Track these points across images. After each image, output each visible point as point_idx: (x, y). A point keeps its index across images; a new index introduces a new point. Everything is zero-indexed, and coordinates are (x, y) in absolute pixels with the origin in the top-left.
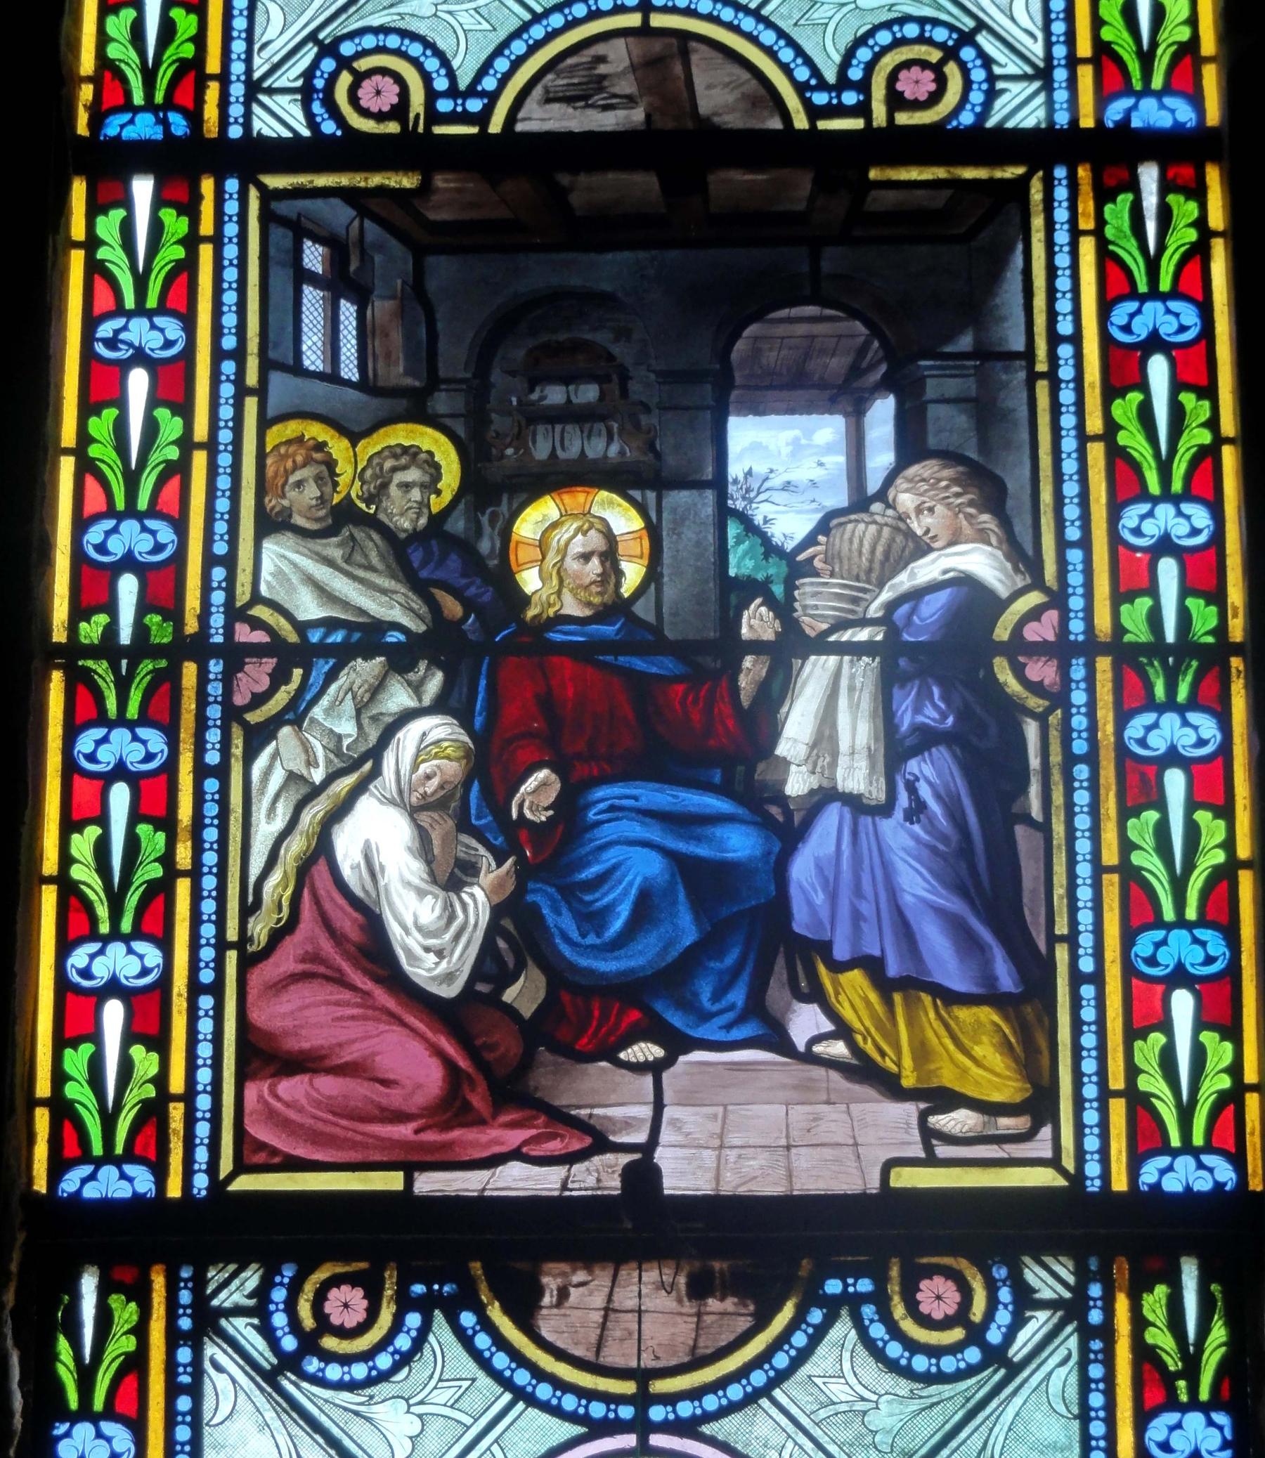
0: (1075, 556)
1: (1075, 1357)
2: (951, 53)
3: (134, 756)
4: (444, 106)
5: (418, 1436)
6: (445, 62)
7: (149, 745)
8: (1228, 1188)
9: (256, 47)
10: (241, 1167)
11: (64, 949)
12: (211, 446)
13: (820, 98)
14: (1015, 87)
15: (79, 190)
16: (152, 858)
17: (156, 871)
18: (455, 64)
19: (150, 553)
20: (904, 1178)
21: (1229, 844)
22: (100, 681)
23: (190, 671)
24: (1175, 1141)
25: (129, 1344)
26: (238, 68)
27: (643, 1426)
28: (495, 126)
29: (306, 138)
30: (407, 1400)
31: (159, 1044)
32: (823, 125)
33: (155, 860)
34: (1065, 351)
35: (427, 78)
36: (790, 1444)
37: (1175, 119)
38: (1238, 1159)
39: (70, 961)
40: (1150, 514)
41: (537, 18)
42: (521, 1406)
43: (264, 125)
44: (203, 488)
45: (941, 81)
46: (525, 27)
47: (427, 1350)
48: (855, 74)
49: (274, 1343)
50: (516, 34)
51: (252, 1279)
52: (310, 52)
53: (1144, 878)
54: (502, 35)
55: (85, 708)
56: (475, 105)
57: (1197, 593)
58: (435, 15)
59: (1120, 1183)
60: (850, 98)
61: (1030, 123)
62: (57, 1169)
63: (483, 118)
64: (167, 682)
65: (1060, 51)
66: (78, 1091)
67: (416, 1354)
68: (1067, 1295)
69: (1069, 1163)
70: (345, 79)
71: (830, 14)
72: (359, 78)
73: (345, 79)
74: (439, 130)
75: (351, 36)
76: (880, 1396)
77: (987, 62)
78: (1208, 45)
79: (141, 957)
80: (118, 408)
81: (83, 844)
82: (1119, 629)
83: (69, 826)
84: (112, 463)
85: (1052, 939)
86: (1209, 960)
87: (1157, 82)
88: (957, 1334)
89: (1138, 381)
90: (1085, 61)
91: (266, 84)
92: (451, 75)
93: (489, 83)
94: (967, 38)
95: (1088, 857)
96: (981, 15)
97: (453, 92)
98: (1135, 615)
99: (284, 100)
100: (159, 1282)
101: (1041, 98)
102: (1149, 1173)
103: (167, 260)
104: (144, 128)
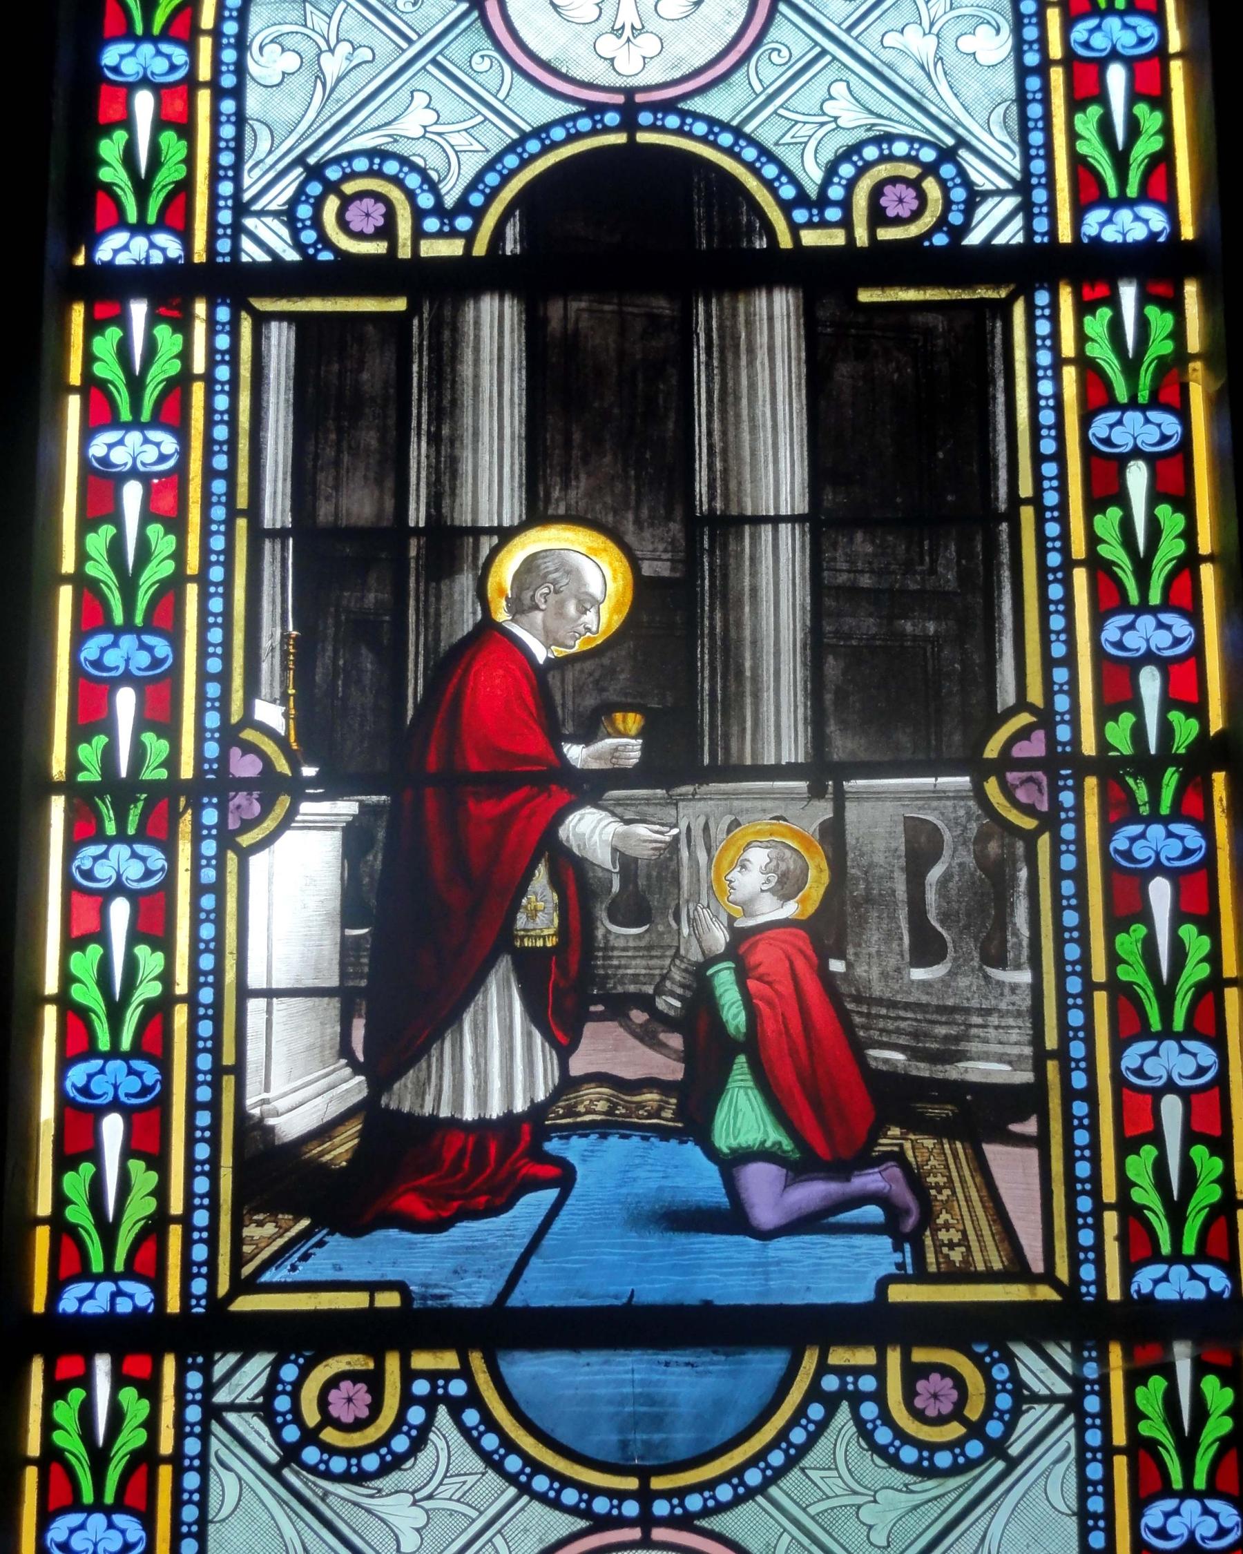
0: (1049, 469)
5: (424, 1527)
8: (1162, 239)
12: (202, 579)
15: (78, 313)
16: (156, 764)
20: (898, 1294)
27: (646, 1521)
29: (293, 263)
37: (1209, 1291)
38: (1230, 1268)
42: (525, 1499)
43: (251, 252)
48: (836, 193)
53: (1115, 574)
55: (69, 1265)
58: (423, 136)
59: (1065, 236)
62: (56, 1290)
66: (79, 1214)
69: (1062, 1273)
79: (123, 1532)
80: (108, 735)
81: (65, 1412)
82: (1103, 743)
83: (71, 944)
85: (1015, 501)
94: (947, 155)
96: (960, 130)
98: (1119, 734)
102: (1144, 1279)
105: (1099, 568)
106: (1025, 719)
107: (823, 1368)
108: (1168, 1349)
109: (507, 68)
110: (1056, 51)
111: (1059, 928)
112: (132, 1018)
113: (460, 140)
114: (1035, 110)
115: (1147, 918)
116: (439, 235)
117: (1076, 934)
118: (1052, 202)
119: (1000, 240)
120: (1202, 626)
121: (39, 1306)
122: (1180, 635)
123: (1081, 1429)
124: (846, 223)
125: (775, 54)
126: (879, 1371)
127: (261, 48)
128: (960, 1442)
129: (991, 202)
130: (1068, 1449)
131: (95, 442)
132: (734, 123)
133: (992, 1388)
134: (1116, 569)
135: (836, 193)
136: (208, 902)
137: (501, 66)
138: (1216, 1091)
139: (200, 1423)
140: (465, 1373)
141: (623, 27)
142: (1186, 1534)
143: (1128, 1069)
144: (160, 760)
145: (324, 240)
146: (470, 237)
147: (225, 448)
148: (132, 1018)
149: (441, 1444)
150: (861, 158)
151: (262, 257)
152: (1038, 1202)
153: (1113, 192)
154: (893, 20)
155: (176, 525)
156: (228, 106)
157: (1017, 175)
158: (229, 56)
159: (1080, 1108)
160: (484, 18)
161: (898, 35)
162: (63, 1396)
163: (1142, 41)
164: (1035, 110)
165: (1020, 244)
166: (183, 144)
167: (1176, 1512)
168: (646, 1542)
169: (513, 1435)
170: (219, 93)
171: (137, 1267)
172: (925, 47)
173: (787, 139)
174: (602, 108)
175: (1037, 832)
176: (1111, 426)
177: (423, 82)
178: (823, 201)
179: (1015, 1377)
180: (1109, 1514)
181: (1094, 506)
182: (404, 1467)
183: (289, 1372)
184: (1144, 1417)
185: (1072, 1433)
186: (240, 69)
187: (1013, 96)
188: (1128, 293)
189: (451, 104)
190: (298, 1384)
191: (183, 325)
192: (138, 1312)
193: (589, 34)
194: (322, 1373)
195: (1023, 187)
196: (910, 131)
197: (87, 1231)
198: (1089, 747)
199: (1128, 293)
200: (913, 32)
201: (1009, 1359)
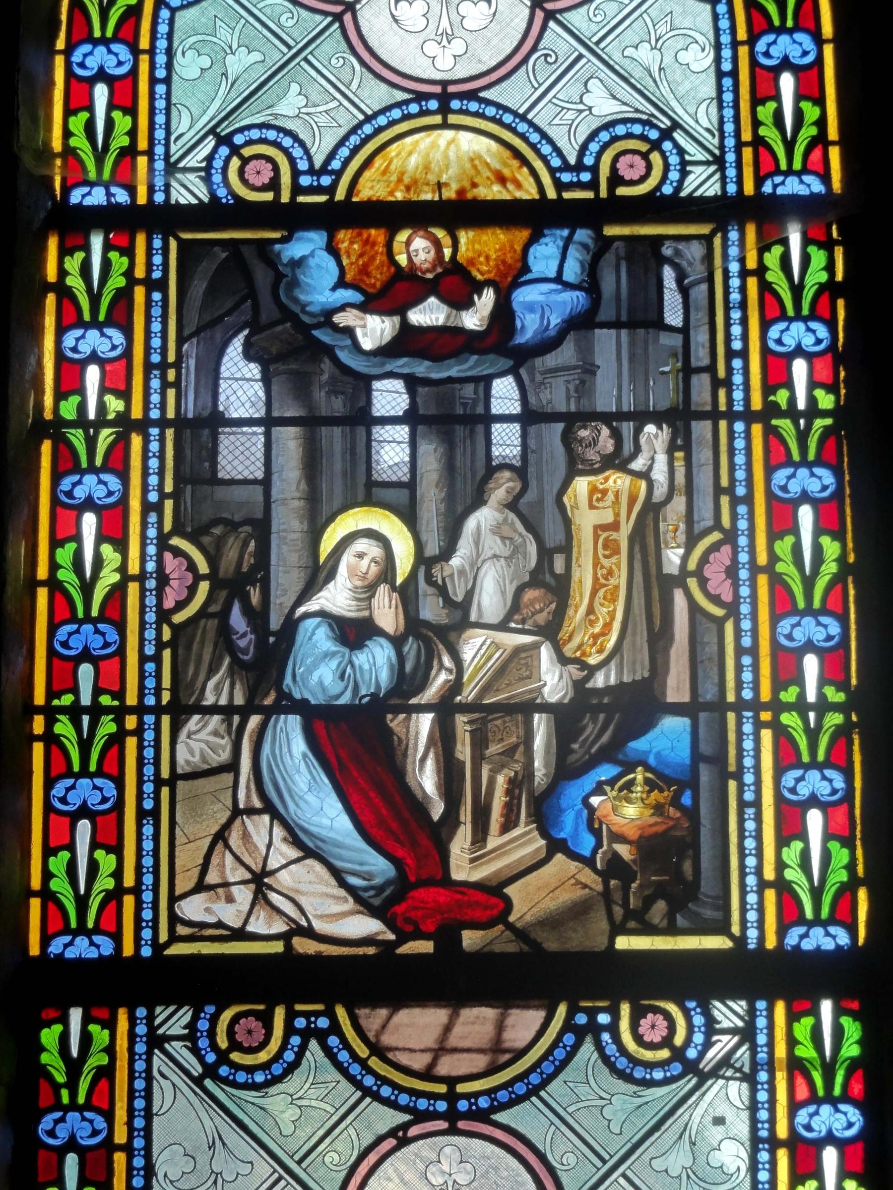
2: (656, 145)
3: (103, 348)
4: (305, 181)
6: (307, 152)
9: (173, 138)
10: (174, 938)
13: (566, 177)
14: (698, 170)
15: (53, 244)
17: (121, 282)
18: (313, 151)
23: (136, 441)
24: (806, 758)
26: (159, 150)
28: (340, 195)
30: (291, 1096)
31: (131, 111)
32: (567, 195)
33: (102, 1051)
34: (737, 363)
35: (292, 161)
36: (553, 1128)
39: (54, 792)
41: (368, 119)
42: (368, 1100)
43: (181, 197)
46: (360, 125)
47: (304, 1061)
49: (201, 1059)
50: (353, 131)
51: (185, 1015)
54: (342, 132)
55: (62, 613)
56: (326, 181)
57: (831, 683)
60: (586, 177)
61: (711, 193)
62: (46, 940)
63: (331, 190)
64: (121, 446)
65: (730, 142)
66: (59, 885)
68: (740, 1024)
71: (573, 117)
72: (245, 161)
74: (301, 199)
75: (241, 130)
76: (613, 1095)
77: (681, 152)
78: (833, 133)
83: (49, 852)
88: (665, 1054)
89: (773, 93)
91: (181, 165)
92: (310, 159)
93: (336, 165)
95: (734, 180)
97: (311, 171)
99: (192, 176)
101: (717, 176)
104: (97, 197)
106: (716, 536)
108: (784, 229)
113: (323, 120)
121: (34, 950)
127: (183, 53)
144: (125, 131)
149: (311, 1059)
160: (343, 28)
161: (634, 49)
165: (716, 196)
169: (361, 152)
173: (556, 121)
174: (427, 96)
181: (782, 841)
193: (416, 40)
194: (227, 1016)
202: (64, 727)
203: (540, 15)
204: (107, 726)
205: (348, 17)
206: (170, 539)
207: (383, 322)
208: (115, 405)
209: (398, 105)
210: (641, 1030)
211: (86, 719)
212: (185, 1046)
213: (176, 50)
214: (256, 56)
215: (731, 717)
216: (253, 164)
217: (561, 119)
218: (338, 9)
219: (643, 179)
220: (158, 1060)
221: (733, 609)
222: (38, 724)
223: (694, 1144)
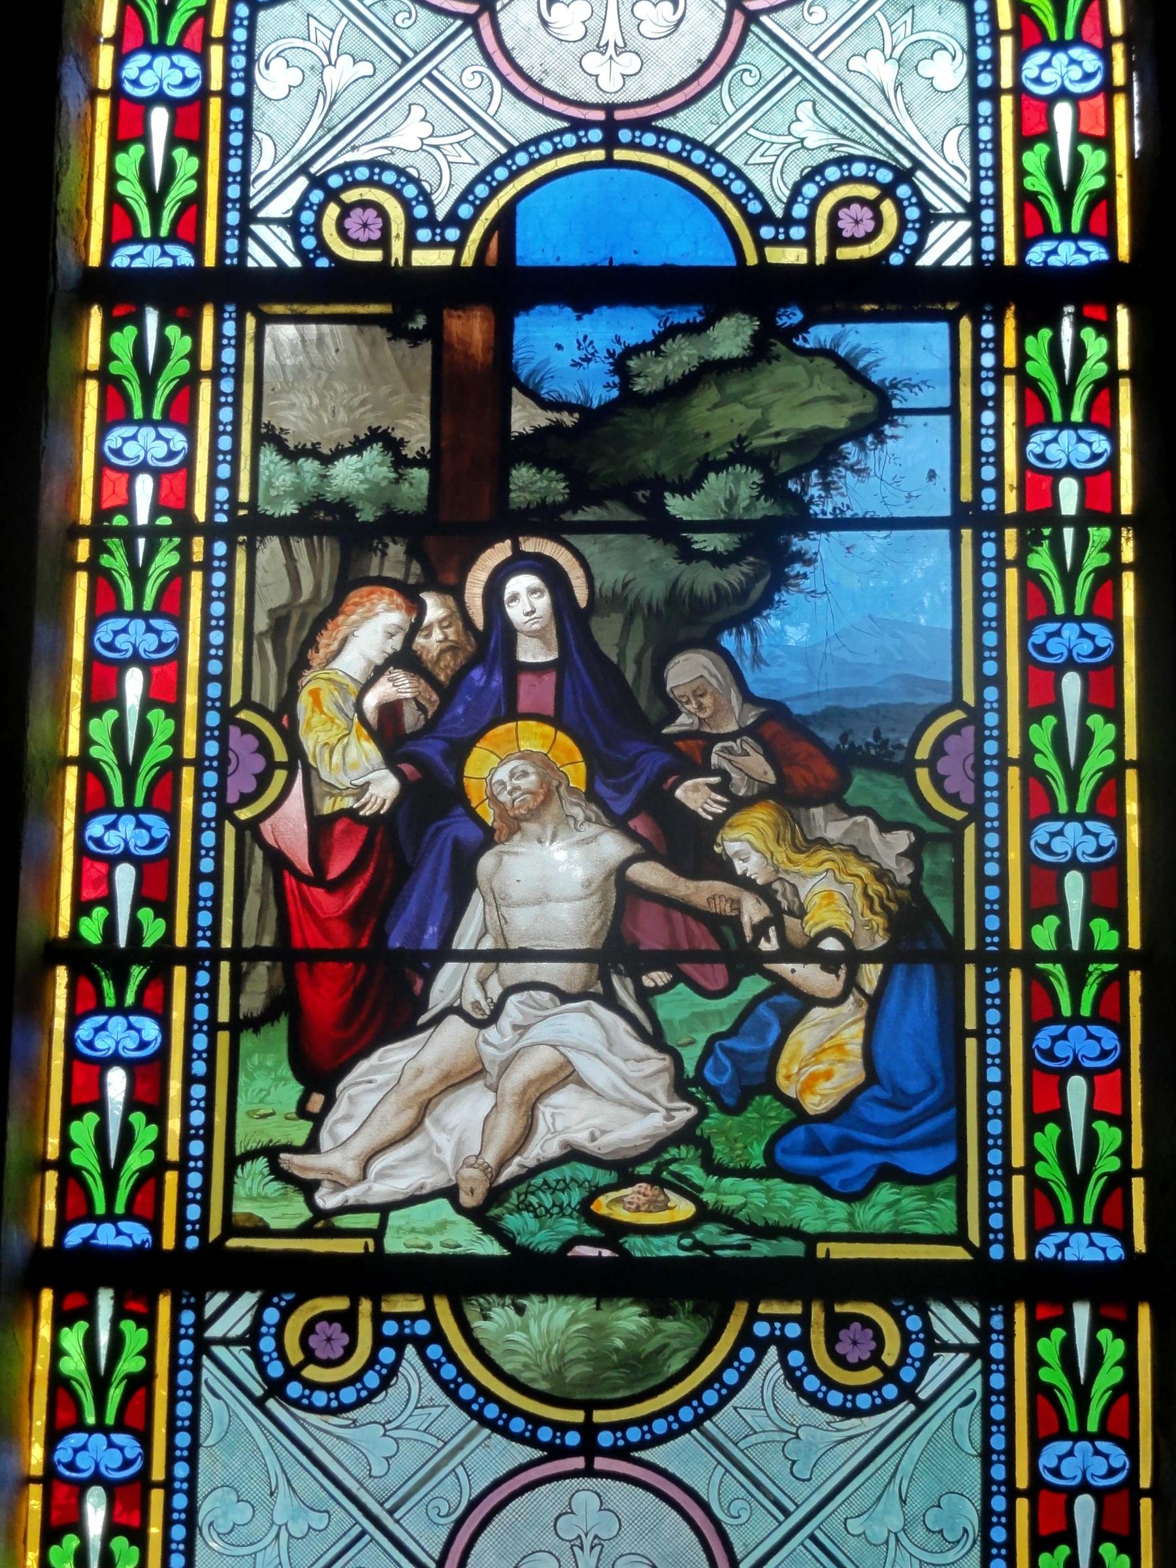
1: (979, 1396)
7: (144, 1034)
11: (74, 1021)
15: (96, 317)
19: (156, 651)
21: (1118, 745)
22: (107, 770)
25: (191, 187)
29: (296, 269)
40: (1064, 1036)
43: (257, 258)
44: (189, 840)
45: (878, 219)
48: (800, 211)
52: (302, 183)
53: (1039, 201)
67: (391, 1379)
69: (974, 1236)
70: (333, 211)
73: (333, 211)
79: (121, 1449)
83: (71, 1113)
84: (137, 198)
86: (1112, 1472)
87: (1077, 415)
90: (1006, 32)
98: (1044, 936)
100: (164, 1304)
103: (162, 568)
105: (1028, 386)
106: (958, 715)
107: (753, 1317)
109: (497, 83)
110: (1007, 81)
111: (979, 617)
112: (115, 1395)
114: (985, 133)
115: (1058, 710)
116: (431, 245)
117: (997, 1001)
118: (1003, 817)
119: (951, 262)
120: (1123, 723)
122: (1107, 1047)
123: (986, 1373)
124: (808, 242)
125: (746, 74)
126: (804, 1320)
128: (878, 1385)
129: (944, 225)
130: (973, 1396)
131: (127, 66)
132: (709, 142)
133: (906, 1338)
134: (1052, 979)
135: (800, 211)
136: (992, 892)
137: (490, 80)
138: (1118, 1073)
139: (192, 1356)
140: (430, 1314)
141: (607, 44)
142: (1066, 654)
143: (1045, 1467)
145: (323, 248)
146: (459, 246)
147: (229, 458)
148: (115, 1395)
150: (824, 178)
151: (268, 263)
152: (950, 646)
153: (1053, 36)
154: (859, 43)
155: (198, 148)
156: (237, 114)
157: (967, 198)
158: (239, 62)
159: (992, 892)
160: (477, 35)
162: (88, 913)
163: (1095, 457)
164: (985, 133)
166: (171, 723)
167: (1058, 633)
168: (609, 163)
170: (229, 102)
171: (136, 1210)
172: (887, 74)
174: (588, 125)
175: (965, 823)
176: (1047, 443)
177: (419, 96)
178: (788, 221)
179: (927, 1327)
180: (1010, 1451)
182: (374, 1401)
183: (271, 1316)
184: (1044, 1364)
185: (979, 1379)
186: (248, 79)
187: (967, 121)
188: (1082, 1313)
189: (447, 118)
190: (281, 1326)
191: (192, 328)
192: (138, 1250)
195: (973, 210)
196: (870, 153)
197: (92, 1175)
198: (1016, 943)
199: (1082, 1313)
200: (875, 56)
201: (923, 1312)
202: (116, 561)
203: (739, 19)
204: (166, 559)
205: (484, 21)
206: (254, 314)
207: (515, 597)
208: (153, 931)
209: (549, 136)
210: (855, 207)
211: (141, 543)
212: (244, 1350)
213: (260, 54)
214: (365, 68)
215: (970, 972)
216: (357, 212)
217: (762, 156)
218: (472, 9)
219: (869, 237)
220: (209, 1370)
221: (976, 814)
222: (83, 550)
223: (905, 1502)
